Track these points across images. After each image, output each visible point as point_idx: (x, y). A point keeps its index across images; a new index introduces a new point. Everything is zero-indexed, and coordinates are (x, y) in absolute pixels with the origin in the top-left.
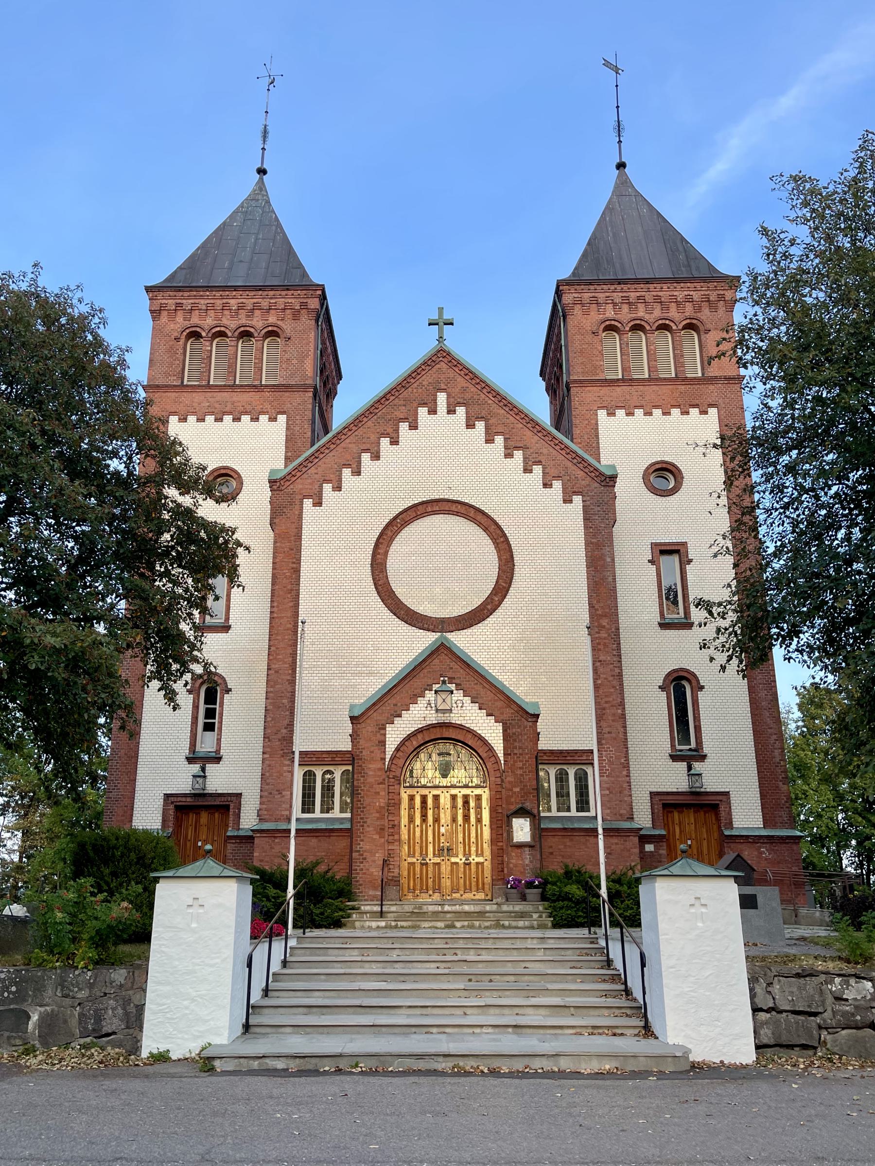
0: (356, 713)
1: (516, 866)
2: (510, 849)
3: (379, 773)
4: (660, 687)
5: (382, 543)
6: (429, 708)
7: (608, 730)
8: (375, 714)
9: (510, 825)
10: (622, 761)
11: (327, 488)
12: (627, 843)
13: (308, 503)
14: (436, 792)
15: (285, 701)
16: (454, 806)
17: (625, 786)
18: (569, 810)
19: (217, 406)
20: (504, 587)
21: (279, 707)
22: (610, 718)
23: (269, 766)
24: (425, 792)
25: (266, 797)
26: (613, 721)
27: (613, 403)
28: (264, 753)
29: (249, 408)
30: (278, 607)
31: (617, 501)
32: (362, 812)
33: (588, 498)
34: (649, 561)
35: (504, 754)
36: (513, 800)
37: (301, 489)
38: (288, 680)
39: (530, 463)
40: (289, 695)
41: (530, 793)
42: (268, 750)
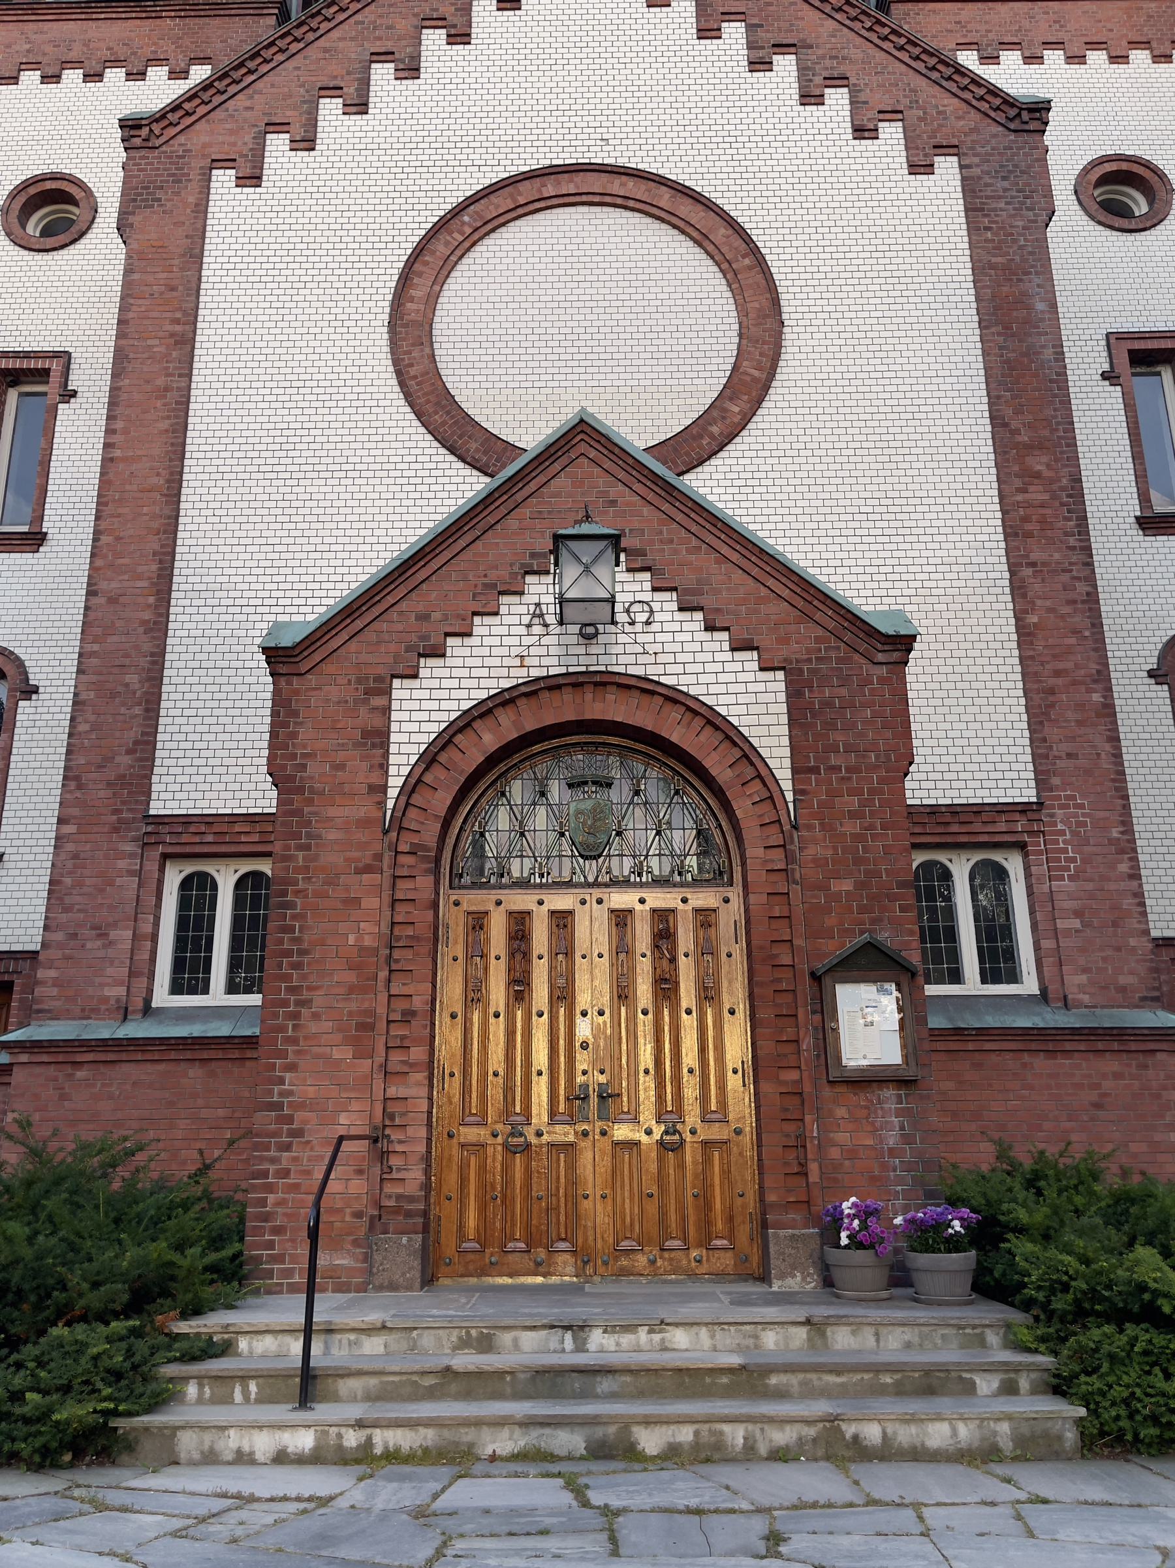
0: (287, 641)
1: (852, 1153)
2: (827, 1092)
3: (362, 836)
4: (1151, 674)
5: (420, 275)
6: (537, 629)
7: (1065, 747)
8: (353, 645)
9: (826, 1009)
10: (1115, 833)
11: (277, 144)
12: (1150, 1073)
13: (223, 179)
14: (562, 901)
15: (132, 679)
16: (622, 948)
17: (1128, 902)
18: (956, 976)
19: (48, 49)
20: (755, 380)
21: (114, 695)
22: (1070, 715)
23: (75, 856)
24: (522, 901)
25: (61, 946)
26: (1080, 723)
27: (991, 36)
28: (61, 821)
29: (122, 53)
30: (126, 432)
31: (1051, 159)
32: (297, 966)
33: (976, 160)
34: (1105, 376)
35: (795, 770)
36: (830, 921)
37: (205, 146)
38: (144, 623)
39: (818, 80)
40: (144, 662)
41: (893, 898)
42: (75, 811)
